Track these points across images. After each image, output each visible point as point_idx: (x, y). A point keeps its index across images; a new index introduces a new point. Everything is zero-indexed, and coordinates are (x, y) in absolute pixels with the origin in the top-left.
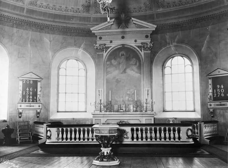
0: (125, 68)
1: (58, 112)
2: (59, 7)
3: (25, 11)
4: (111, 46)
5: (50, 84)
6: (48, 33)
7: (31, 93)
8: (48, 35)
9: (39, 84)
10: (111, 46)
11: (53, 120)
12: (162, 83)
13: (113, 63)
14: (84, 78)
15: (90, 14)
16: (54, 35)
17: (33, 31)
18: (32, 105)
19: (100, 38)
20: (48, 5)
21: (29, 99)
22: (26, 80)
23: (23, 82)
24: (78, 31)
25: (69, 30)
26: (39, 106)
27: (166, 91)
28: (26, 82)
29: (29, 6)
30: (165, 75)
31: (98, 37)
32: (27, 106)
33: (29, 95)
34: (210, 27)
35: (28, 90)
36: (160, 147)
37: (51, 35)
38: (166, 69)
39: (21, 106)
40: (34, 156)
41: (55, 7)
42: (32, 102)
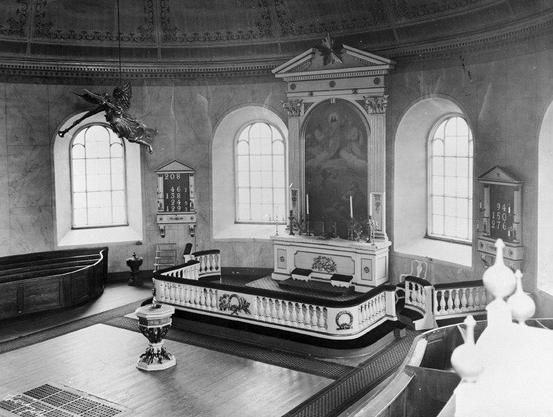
0: (338, 146)
1: (73, 229)
2: (216, 35)
3: (29, 49)
4: (313, 103)
5: (211, 177)
6: (204, 84)
7: (179, 196)
8: (203, 89)
9: (192, 179)
10: (313, 103)
11: (88, 247)
12: (423, 175)
13: (317, 136)
14: (122, 160)
15: (24, 38)
16: (214, 87)
17: (176, 84)
18: (179, 216)
19: (293, 87)
20: (207, 34)
21: (176, 205)
22: (169, 175)
23: (164, 178)
24: (149, 75)
25: (240, 74)
26: (192, 218)
27: (434, 193)
28: (169, 177)
29: (35, 39)
30: (432, 157)
31: (290, 84)
32: (172, 219)
33: (176, 199)
34: (493, 63)
35: (173, 190)
36: (212, 323)
37: (209, 87)
38: (240, 144)
39: (192, 218)
40: (106, 312)
41: (73, 33)
42: (181, 211)
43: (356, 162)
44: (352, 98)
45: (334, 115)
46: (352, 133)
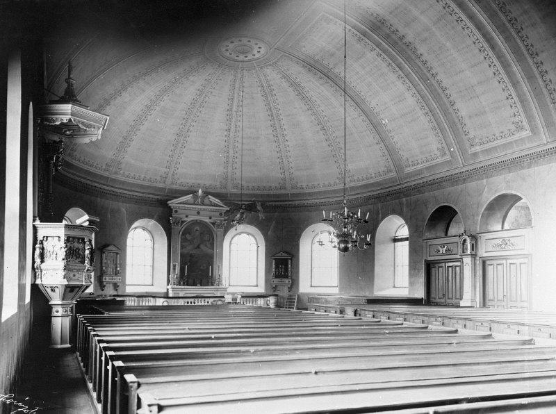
43: (210, 251)
44: (207, 220)
45: (197, 228)
46: (207, 237)
